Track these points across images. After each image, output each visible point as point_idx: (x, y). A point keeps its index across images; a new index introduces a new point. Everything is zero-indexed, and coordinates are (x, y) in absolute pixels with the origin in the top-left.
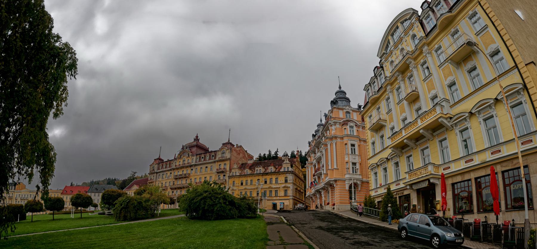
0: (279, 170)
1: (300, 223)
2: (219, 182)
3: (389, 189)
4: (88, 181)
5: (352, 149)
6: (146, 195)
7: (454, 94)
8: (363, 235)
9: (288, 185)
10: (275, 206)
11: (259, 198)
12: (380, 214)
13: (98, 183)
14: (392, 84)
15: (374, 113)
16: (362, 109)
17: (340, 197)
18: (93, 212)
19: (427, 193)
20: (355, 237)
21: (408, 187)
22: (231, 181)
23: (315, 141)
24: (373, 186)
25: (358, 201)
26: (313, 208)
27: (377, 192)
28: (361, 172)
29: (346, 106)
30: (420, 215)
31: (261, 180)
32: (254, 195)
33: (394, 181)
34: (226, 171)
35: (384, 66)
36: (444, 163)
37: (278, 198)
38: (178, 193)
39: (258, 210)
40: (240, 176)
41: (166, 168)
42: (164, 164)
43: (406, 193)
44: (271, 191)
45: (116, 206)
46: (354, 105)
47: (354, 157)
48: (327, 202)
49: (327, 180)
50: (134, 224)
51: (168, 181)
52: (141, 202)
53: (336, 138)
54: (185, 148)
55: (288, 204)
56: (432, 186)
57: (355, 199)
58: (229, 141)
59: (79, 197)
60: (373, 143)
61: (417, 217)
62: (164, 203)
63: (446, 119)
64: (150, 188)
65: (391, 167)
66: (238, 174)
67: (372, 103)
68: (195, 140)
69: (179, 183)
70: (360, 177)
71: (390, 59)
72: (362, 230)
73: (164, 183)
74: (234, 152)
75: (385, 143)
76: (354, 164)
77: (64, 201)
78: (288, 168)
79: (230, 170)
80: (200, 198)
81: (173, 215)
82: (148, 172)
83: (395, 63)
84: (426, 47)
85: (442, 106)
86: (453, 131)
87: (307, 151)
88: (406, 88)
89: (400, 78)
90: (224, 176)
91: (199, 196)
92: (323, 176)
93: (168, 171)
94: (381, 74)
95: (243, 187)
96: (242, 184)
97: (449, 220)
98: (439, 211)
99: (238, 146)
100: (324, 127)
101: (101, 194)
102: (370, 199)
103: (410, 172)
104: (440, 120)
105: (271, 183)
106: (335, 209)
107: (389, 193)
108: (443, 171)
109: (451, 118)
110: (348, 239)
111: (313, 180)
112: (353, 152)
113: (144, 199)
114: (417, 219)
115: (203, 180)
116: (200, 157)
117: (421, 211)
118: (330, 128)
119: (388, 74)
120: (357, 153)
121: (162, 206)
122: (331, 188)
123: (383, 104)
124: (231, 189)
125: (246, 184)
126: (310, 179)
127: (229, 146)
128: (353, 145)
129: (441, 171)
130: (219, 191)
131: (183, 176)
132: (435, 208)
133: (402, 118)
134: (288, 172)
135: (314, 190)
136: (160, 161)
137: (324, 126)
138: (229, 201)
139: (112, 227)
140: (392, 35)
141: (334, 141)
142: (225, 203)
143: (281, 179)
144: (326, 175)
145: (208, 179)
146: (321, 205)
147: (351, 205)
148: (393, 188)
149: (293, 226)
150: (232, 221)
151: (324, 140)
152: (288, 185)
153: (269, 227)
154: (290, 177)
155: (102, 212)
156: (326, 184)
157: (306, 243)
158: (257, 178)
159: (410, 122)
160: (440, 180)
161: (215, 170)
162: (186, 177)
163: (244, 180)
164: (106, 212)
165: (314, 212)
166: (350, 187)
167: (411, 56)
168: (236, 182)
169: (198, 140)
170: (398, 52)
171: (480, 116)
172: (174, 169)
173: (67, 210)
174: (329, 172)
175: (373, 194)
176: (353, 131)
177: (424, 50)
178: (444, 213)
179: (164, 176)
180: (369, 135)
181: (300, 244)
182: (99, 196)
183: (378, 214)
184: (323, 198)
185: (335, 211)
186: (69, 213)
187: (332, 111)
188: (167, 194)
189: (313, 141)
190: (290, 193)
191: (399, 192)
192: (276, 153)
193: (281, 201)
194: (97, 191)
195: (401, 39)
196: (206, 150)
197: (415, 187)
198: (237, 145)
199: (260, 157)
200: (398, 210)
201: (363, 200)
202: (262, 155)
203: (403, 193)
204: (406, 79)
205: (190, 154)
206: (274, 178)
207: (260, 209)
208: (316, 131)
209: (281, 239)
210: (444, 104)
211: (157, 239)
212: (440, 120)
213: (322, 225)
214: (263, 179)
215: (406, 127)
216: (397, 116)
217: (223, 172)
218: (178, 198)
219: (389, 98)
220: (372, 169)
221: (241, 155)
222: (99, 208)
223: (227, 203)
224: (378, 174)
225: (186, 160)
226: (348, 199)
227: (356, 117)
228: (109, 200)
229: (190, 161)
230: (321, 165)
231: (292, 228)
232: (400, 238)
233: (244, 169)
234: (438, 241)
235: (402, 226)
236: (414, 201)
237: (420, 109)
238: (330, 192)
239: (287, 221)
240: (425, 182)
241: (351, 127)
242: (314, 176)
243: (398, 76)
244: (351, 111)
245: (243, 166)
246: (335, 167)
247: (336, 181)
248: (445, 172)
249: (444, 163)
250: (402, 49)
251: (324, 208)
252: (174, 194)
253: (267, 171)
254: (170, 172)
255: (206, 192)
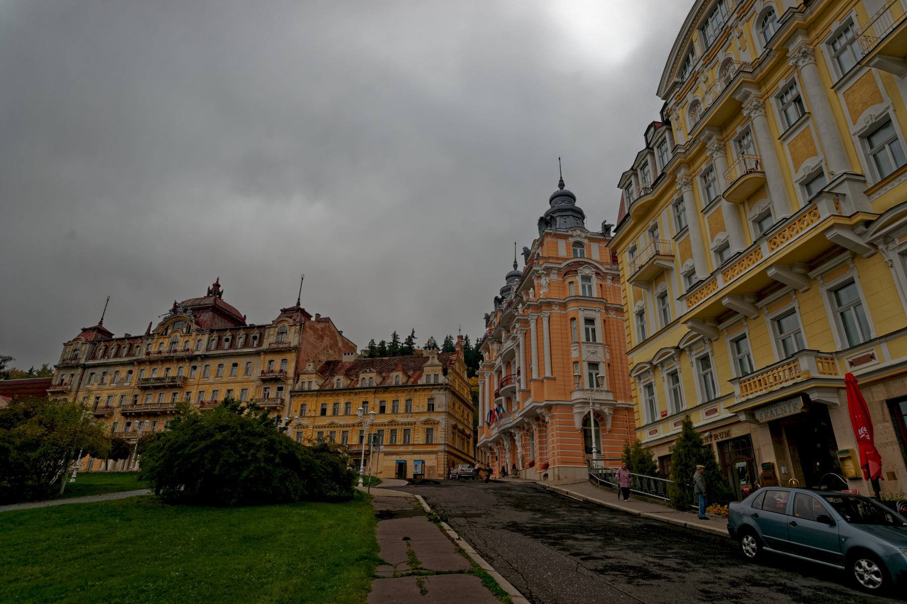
0: (416, 381)
1: (465, 516)
2: (265, 404)
3: (687, 425)
5: (587, 330)
6: (30, 430)
7: (880, 156)
8: (628, 547)
9: (434, 417)
10: (401, 469)
11: (364, 448)
12: (670, 491)
14: (690, 163)
15: (643, 241)
16: (613, 234)
17: (561, 447)
19: (806, 433)
20: (610, 554)
21: (743, 417)
22: (297, 403)
24: (643, 418)
25: (609, 455)
27: (657, 434)
28: (612, 383)
29: (574, 228)
30: (793, 491)
31: (371, 405)
32: (354, 440)
33: (699, 402)
34: (287, 378)
35: (672, 119)
36: (710, 402)
37: (410, 449)
38: (145, 427)
39: (361, 480)
40: (321, 392)
41: (116, 356)
42: (114, 345)
43: (736, 432)
44: (393, 432)
46: (593, 225)
47: (592, 349)
48: (530, 459)
49: (528, 404)
51: (119, 393)
53: (549, 304)
54: (180, 310)
55: (434, 463)
56: (818, 413)
57: (599, 452)
58: (299, 304)
60: (641, 314)
61: (782, 496)
63: (852, 228)
65: (688, 368)
66: (317, 388)
67: (636, 217)
68: (210, 292)
69: (152, 400)
70: (610, 397)
71: (690, 98)
72: (623, 533)
73: (104, 397)
74: (310, 332)
75: (670, 311)
76: (593, 365)
78: (436, 376)
79: (297, 375)
80: (202, 444)
82: (53, 362)
83: (703, 107)
84: (800, 39)
85: (839, 198)
86: (875, 259)
87: (482, 336)
88: (728, 167)
89: (713, 144)
90: (280, 389)
91: (203, 438)
93: (123, 364)
94: (664, 141)
95: (325, 421)
96: (324, 412)
97: (898, 506)
98: (856, 479)
99: (319, 319)
100: (521, 280)
102: (638, 451)
103: (745, 376)
104: (829, 236)
105: (394, 411)
106: (550, 478)
107: (690, 436)
108: (850, 370)
109: (868, 224)
110: (588, 557)
111: (495, 406)
112: (591, 336)
113: (18, 442)
114: (784, 501)
115: (221, 398)
116: (220, 338)
117: (794, 480)
118: (536, 282)
119: (681, 138)
120: (599, 339)
121: (82, 464)
122: (539, 426)
123: (665, 218)
124: (294, 423)
125: (335, 413)
126: (486, 404)
127: (298, 317)
128: (590, 321)
129: (842, 369)
130: (260, 429)
131: (167, 382)
132: (839, 471)
133: (714, 245)
134: (436, 386)
138: (282, 456)
140: (703, 28)
141: (545, 314)
142: (268, 460)
143: (420, 402)
144: (527, 393)
145: (236, 395)
146: (514, 467)
147: (590, 468)
148: (699, 420)
149: (444, 524)
150: (285, 509)
152: (434, 417)
154: (441, 399)
156: (524, 415)
158: (363, 398)
159: (739, 253)
160: (844, 393)
161: (256, 374)
162: (174, 385)
163: (330, 402)
165: (498, 485)
166: (586, 421)
167: (748, 78)
168: (308, 408)
169: (220, 294)
170: (714, 74)
171: (891, 246)
172: (140, 362)
174: (532, 386)
175: (645, 437)
176: (590, 287)
178: (876, 487)
179: (108, 379)
181: (461, 572)
183: (665, 490)
184: (519, 450)
187: (540, 243)
189: (495, 314)
190: (440, 436)
191: (718, 432)
192: (410, 340)
193: (417, 457)
195: (726, 32)
196: (236, 321)
197: (763, 417)
198: (318, 315)
199: (372, 347)
200: (719, 478)
201: (621, 453)
202: (377, 343)
203: (728, 434)
204: (731, 143)
205: (194, 327)
206: (402, 398)
207: (364, 477)
208: (503, 291)
210: (845, 189)
211: (29, 570)
212: (829, 236)
213: (518, 520)
214: (377, 402)
215: (725, 267)
216: (703, 241)
217: (276, 380)
218: (141, 442)
219: (681, 200)
221: (327, 341)
223: (277, 460)
224: (655, 389)
225: (181, 341)
226: (581, 451)
227: (596, 253)
229: (191, 345)
230: (514, 371)
231: (443, 530)
232: (740, 558)
234: (876, 574)
235: (739, 523)
236: (766, 452)
237: (768, 214)
238: (536, 434)
239: (433, 507)
240: (793, 401)
241: (586, 278)
242: (497, 395)
243: (709, 138)
244: (586, 241)
245: (328, 369)
246: (548, 374)
247: (549, 407)
248: (857, 371)
249: (852, 348)
250: (728, 62)
251: (523, 475)
252: (130, 429)
254: (129, 368)
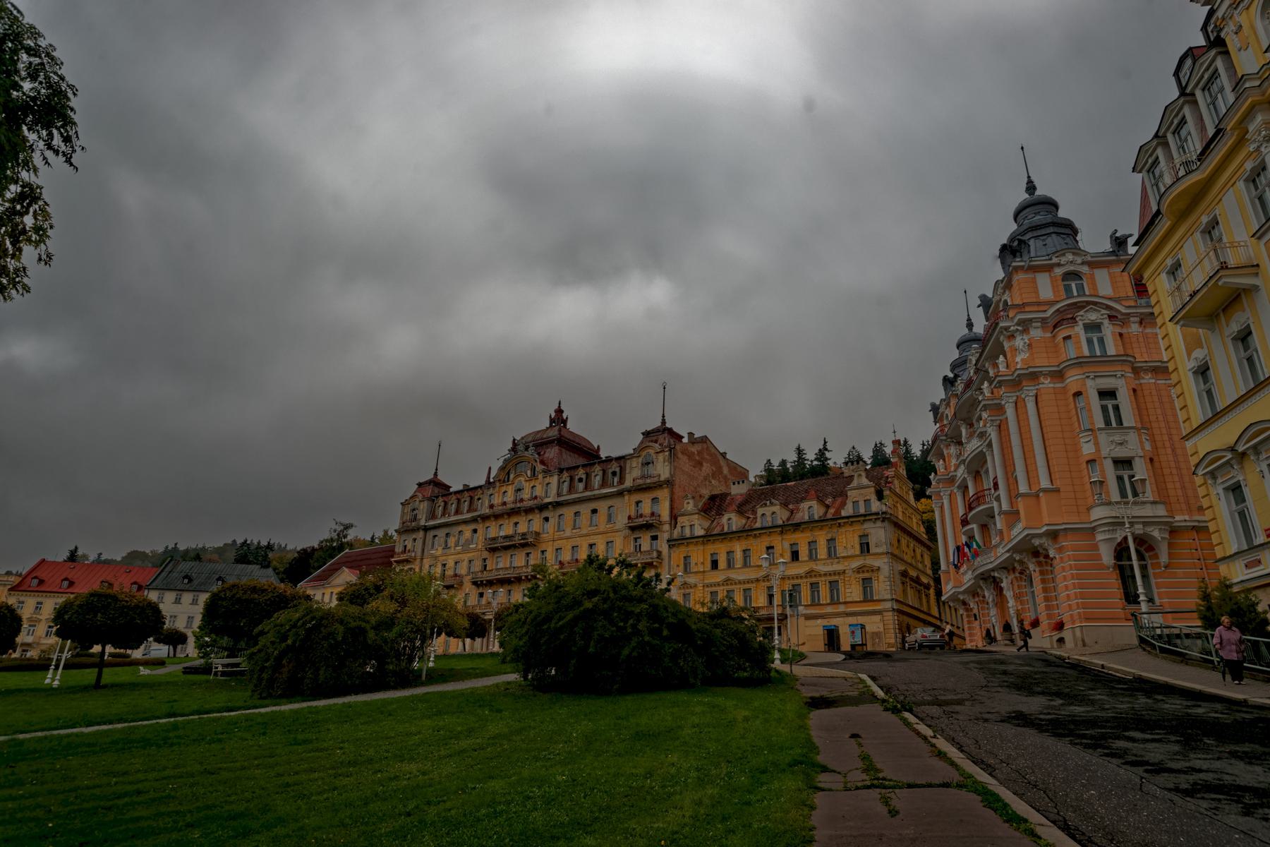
0: (838, 512)
4: (157, 546)
6: (382, 606)
8: (1234, 755)
9: (870, 561)
10: (832, 638)
11: (776, 612)
13: (197, 555)
18: (160, 663)
22: (679, 554)
23: (953, 402)
24: (1230, 541)
26: (975, 640)
31: (778, 549)
32: (760, 600)
34: (661, 523)
35: (1228, 35)
37: (842, 608)
38: (498, 599)
39: (777, 656)
40: (708, 538)
41: (457, 512)
42: (453, 499)
44: (814, 586)
45: (262, 641)
46: (1094, 241)
47: (1117, 438)
49: (1018, 532)
50: (329, 708)
51: (466, 557)
52: (363, 631)
53: (1034, 377)
54: (521, 447)
55: (881, 628)
57: (1151, 600)
58: (664, 422)
59: (100, 602)
60: (1203, 371)
62: (449, 634)
64: (398, 580)
66: (702, 533)
68: (552, 421)
69: (504, 564)
70: (1161, 511)
72: (1220, 732)
73: (451, 563)
76: (1123, 463)
77: (18, 620)
78: (867, 501)
79: (674, 518)
80: (570, 615)
81: (477, 676)
82: (394, 525)
87: (929, 437)
90: (655, 538)
91: (570, 608)
92: (1000, 523)
93: (465, 522)
95: (718, 577)
96: (715, 564)
100: (980, 347)
101: (204, 597)
105: (812, 556)
106: (1069, 643)
110: (1158, 769)
112: (1113, 419)
113: (373, 620)
115: (583, 555)
116: (572, 479)
118: (1006, 345)
120: (1129, 419)
122: (1040, 564)
124: (678, 582)
125: (730, 565)
126: (949, 539)
127: (665, 439)
130: (638, 592)
131: (517, 540)
134: (868, 517)
135: (969, 576)
136: (436, 489)
137: (982, 341)
139: (234, 723)
141: (1029, 392)
142: (655, 633)
143: (848, 541)
144: (1013, 516)
145: (600, 550)
147: (1140, 627)
149: (907, 715)
150: (682, 696)
151: (987, 394)
152: (870, 561)
153: (816, 716)
154: (879, 535)
155: (200, 662)
156: (1015, 549)
157: (967, 783)
158: (765, 541)
161: (621, 521)
162: (525, 543)
163: (721, 550)
164: (219, 662)
166: (1121, 552)
168: (693, 561)
169: (565, 422)
172: (485, 518)
173: (33, 654)
176: (1101, 341)
177: (1251, 128)
179: (452, 541)
180: (1174, 343)
181: (946, 785)
182: (195, 602)
184: (1011, 603)
185: (1070, 651)
186: (42, 666)
188: (458, 599)
189: (947, 402)
190: (883, 588)
192: (822, 454)
193: (852, 620)
194: (189, 583)
196: (589, 455)
198: (691, 434)
199: (769, 470)
202: (776, 464)
205: (540, 467)
206: (822, 538)
208: (954, 366)
209: (870, 768)
213: (1024, 709)
214: (787, 545)
217: (648, 526)
218: (498, 617)
220: (1213, 475)
221: (707, 468)
222: (191, 649)
223: (665, 633)
225: (527, 487)
228: (231, 617)
229: (539, 491)
230: (987, 484)
231: (907, 723)
233: (720, 514)
238: (1037, 578)
239: (887, 690)
241: (1094, 327)
242: (965, 522)
245: (714, 505)
246: (1045, 483)
247: (1054, 535)
252: (484, 601)
253: (798, 518)
254: (473, 526)
255: (591, 594)
